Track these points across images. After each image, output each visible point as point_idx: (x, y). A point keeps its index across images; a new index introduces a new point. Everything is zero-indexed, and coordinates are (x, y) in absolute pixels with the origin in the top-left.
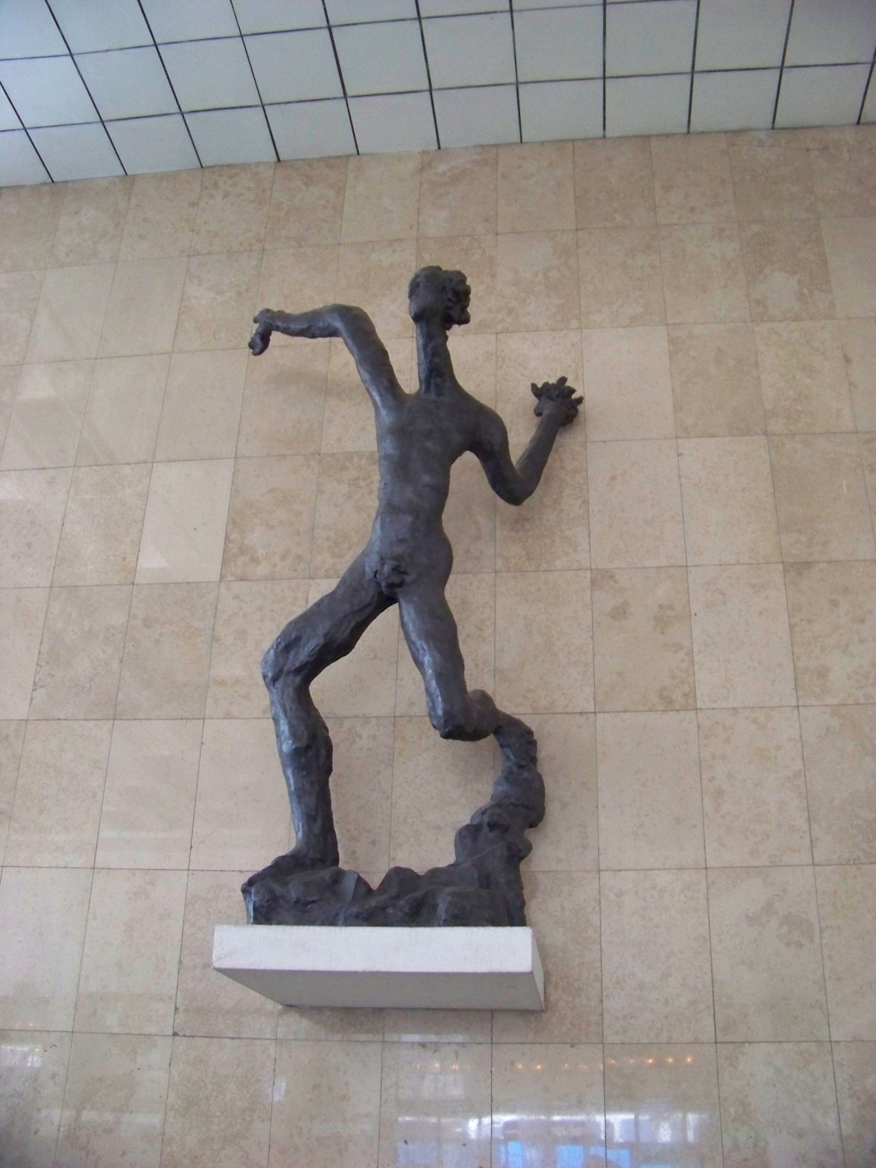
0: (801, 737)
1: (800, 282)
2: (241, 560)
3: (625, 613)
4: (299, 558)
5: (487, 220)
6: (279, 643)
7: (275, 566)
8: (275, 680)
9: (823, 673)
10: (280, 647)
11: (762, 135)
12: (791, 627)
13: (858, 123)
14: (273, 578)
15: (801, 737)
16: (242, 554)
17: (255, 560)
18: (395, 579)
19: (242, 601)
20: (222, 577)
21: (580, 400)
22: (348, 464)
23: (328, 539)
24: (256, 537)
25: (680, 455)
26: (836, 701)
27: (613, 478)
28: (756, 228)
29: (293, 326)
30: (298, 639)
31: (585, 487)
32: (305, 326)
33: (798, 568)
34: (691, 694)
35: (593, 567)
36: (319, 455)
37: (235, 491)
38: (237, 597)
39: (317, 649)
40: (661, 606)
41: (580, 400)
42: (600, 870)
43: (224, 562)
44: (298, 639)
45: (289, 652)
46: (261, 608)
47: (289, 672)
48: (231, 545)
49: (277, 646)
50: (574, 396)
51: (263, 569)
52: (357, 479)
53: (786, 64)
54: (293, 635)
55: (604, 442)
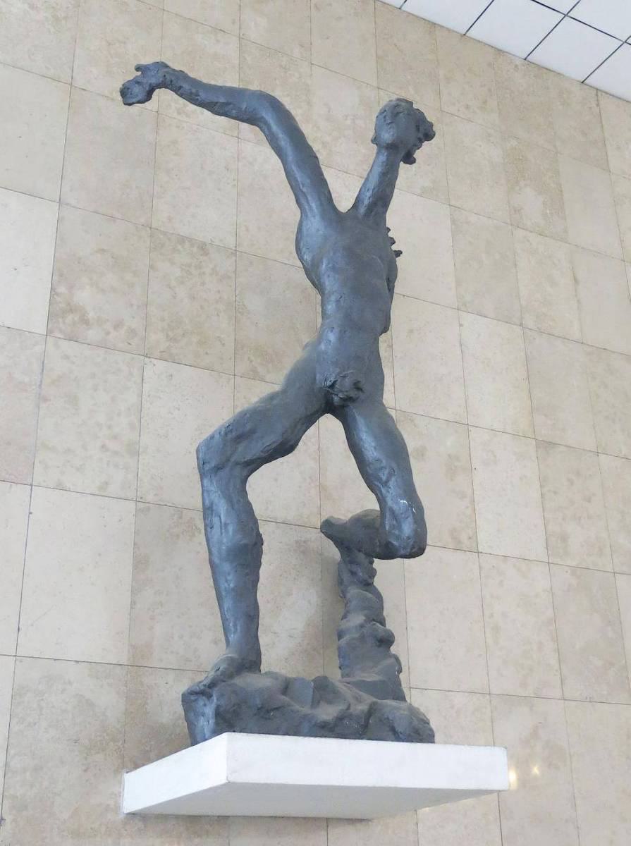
0: (551, 589)
1: (544, 203)
2: (70, 318)
3: (423, 455)
4: (132, 332)
5: (302, 46)
6: (231, 431)
7: (108, 333)
8: (218, 468)
9: (564, 538)
10: (230, 436)
11: (518, 62)
12: (542, 495)
13: (582, 82)
14: (102, 345)
15: (551, 589)
16: (71, 311)
17: (85, 321)
18: (353, 394)
19: (74, 363)
20: (49, 333)
21: (398, 253)
22: (179, 247)
23: (163, 320)
24: (85, 296)
25: (461, 325)
26: (574, 564)
27: (411, 331)
28: (514, 143)
29: (202, 96)
30: (253, 431)
31: (55, 278)
32: (222, 100)
33: (546, 446)
34: (474, 537)
35: (398, 408)
36: (151, 228)
37: (60, 239)
38: (67, 357)
39: (273, 446)
40: (449, 456)
41: (398, 253)
42: (410, 688)
43: (51, 315)
44: (253, 431)
45: (239, 443)
46: (93, 376)
47: (237, 464)
48: (58, 299)
49: (226, 434)
50: (394, 247)
51: (93, 334)
52: (190, 266)
53: (569, 14)
54: (248, 427)
55: (404, 296)
